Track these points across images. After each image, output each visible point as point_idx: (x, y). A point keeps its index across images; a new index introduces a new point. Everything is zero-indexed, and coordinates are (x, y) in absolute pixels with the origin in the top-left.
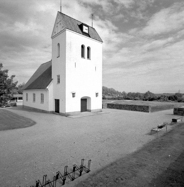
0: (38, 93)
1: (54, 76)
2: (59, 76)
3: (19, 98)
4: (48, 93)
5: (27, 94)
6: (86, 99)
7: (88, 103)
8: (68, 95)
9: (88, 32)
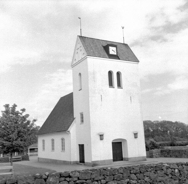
0: (57, 138)
1: (77, 115)
2: (82, 115)
3: (30, 149)
4: (70, 136)
5: (44, 141)
6: (121, 143)
7: (124, 146)
8: (95, 138)
9: (117, 53)
